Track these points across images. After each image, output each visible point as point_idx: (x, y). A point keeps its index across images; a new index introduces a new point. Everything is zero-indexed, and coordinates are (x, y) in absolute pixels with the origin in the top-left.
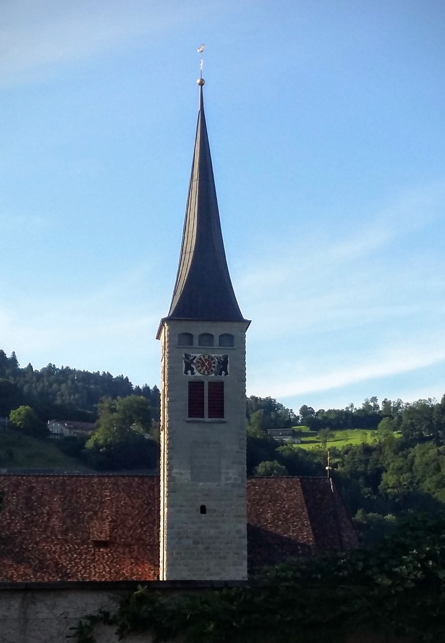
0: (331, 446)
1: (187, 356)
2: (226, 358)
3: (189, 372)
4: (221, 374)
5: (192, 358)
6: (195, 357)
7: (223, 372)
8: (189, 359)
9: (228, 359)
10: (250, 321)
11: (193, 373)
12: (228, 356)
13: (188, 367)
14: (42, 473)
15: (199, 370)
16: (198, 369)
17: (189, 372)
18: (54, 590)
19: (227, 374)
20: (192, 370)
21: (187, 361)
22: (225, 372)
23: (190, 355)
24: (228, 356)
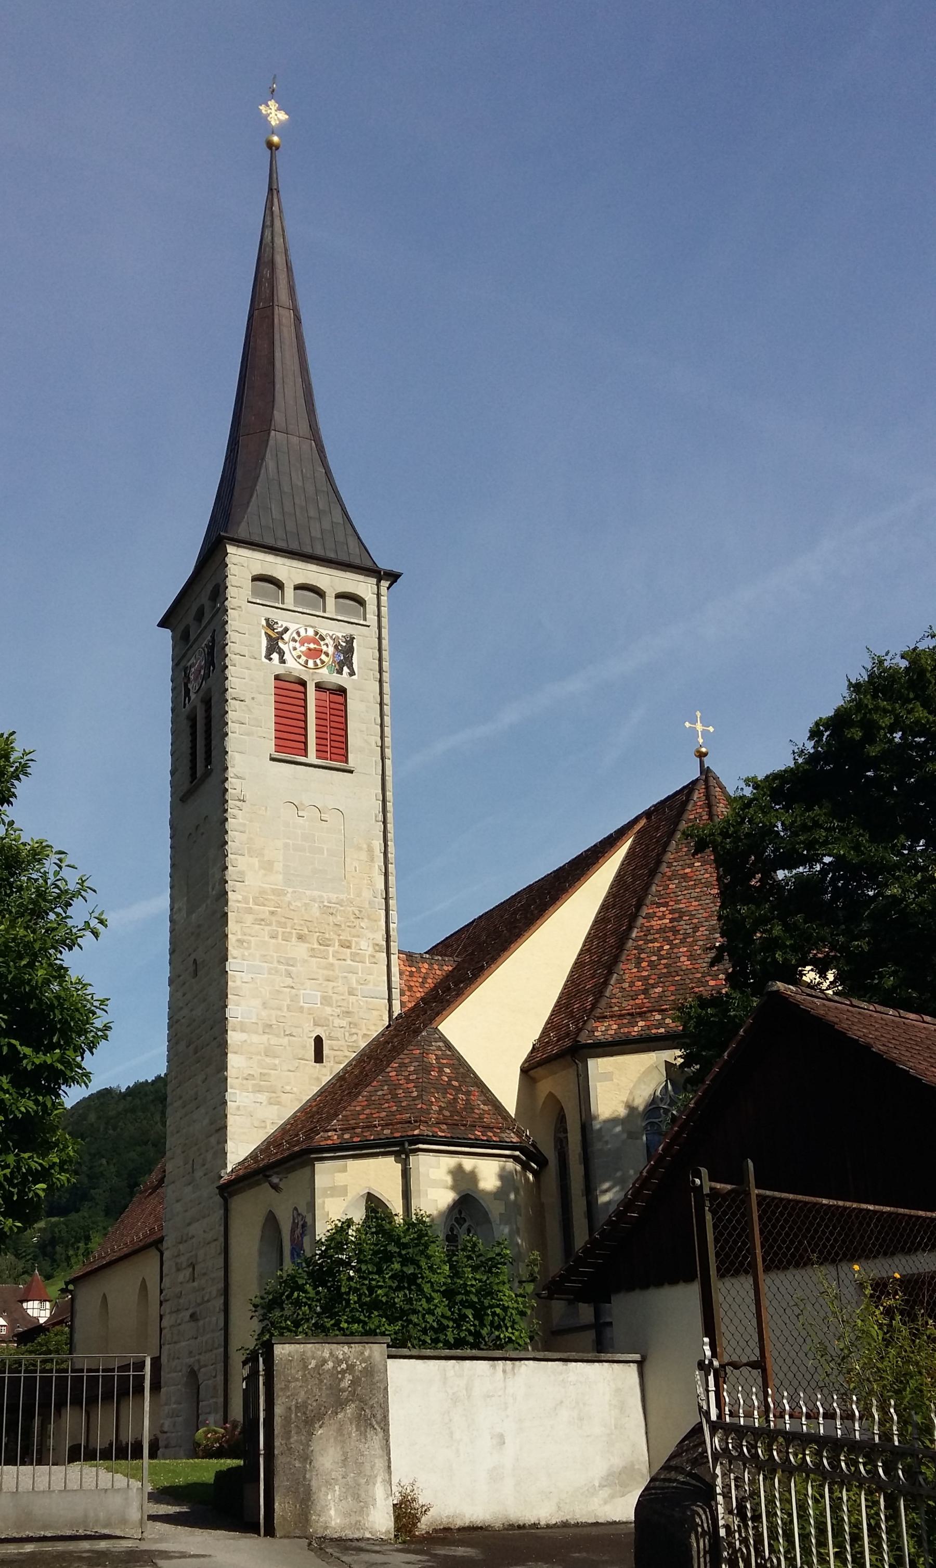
0: (808, 731)
1: (270, 624)
2: (350, 640)
3: (275, 656)
4: (340, 672)
5: (280, 630)
6: (286, 630)
7: (346, 670)
8: (273, 630)
9: (355, 644)
10: (728, 1270)
11: (283, 661)
12: (354, 638)
13: (273, 647)
14: (866, 911)
15: (303, 663)
16: (300, 661)
17: (275, 656)
18: (142, 1250)
19: (352, 673)
20: (281, 653)
21: (270, 632)
22: (348, 668)
23: (277, 623)
24: (354, 638)
